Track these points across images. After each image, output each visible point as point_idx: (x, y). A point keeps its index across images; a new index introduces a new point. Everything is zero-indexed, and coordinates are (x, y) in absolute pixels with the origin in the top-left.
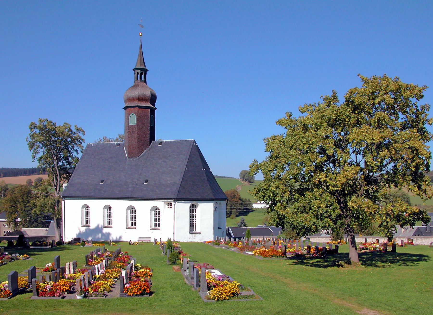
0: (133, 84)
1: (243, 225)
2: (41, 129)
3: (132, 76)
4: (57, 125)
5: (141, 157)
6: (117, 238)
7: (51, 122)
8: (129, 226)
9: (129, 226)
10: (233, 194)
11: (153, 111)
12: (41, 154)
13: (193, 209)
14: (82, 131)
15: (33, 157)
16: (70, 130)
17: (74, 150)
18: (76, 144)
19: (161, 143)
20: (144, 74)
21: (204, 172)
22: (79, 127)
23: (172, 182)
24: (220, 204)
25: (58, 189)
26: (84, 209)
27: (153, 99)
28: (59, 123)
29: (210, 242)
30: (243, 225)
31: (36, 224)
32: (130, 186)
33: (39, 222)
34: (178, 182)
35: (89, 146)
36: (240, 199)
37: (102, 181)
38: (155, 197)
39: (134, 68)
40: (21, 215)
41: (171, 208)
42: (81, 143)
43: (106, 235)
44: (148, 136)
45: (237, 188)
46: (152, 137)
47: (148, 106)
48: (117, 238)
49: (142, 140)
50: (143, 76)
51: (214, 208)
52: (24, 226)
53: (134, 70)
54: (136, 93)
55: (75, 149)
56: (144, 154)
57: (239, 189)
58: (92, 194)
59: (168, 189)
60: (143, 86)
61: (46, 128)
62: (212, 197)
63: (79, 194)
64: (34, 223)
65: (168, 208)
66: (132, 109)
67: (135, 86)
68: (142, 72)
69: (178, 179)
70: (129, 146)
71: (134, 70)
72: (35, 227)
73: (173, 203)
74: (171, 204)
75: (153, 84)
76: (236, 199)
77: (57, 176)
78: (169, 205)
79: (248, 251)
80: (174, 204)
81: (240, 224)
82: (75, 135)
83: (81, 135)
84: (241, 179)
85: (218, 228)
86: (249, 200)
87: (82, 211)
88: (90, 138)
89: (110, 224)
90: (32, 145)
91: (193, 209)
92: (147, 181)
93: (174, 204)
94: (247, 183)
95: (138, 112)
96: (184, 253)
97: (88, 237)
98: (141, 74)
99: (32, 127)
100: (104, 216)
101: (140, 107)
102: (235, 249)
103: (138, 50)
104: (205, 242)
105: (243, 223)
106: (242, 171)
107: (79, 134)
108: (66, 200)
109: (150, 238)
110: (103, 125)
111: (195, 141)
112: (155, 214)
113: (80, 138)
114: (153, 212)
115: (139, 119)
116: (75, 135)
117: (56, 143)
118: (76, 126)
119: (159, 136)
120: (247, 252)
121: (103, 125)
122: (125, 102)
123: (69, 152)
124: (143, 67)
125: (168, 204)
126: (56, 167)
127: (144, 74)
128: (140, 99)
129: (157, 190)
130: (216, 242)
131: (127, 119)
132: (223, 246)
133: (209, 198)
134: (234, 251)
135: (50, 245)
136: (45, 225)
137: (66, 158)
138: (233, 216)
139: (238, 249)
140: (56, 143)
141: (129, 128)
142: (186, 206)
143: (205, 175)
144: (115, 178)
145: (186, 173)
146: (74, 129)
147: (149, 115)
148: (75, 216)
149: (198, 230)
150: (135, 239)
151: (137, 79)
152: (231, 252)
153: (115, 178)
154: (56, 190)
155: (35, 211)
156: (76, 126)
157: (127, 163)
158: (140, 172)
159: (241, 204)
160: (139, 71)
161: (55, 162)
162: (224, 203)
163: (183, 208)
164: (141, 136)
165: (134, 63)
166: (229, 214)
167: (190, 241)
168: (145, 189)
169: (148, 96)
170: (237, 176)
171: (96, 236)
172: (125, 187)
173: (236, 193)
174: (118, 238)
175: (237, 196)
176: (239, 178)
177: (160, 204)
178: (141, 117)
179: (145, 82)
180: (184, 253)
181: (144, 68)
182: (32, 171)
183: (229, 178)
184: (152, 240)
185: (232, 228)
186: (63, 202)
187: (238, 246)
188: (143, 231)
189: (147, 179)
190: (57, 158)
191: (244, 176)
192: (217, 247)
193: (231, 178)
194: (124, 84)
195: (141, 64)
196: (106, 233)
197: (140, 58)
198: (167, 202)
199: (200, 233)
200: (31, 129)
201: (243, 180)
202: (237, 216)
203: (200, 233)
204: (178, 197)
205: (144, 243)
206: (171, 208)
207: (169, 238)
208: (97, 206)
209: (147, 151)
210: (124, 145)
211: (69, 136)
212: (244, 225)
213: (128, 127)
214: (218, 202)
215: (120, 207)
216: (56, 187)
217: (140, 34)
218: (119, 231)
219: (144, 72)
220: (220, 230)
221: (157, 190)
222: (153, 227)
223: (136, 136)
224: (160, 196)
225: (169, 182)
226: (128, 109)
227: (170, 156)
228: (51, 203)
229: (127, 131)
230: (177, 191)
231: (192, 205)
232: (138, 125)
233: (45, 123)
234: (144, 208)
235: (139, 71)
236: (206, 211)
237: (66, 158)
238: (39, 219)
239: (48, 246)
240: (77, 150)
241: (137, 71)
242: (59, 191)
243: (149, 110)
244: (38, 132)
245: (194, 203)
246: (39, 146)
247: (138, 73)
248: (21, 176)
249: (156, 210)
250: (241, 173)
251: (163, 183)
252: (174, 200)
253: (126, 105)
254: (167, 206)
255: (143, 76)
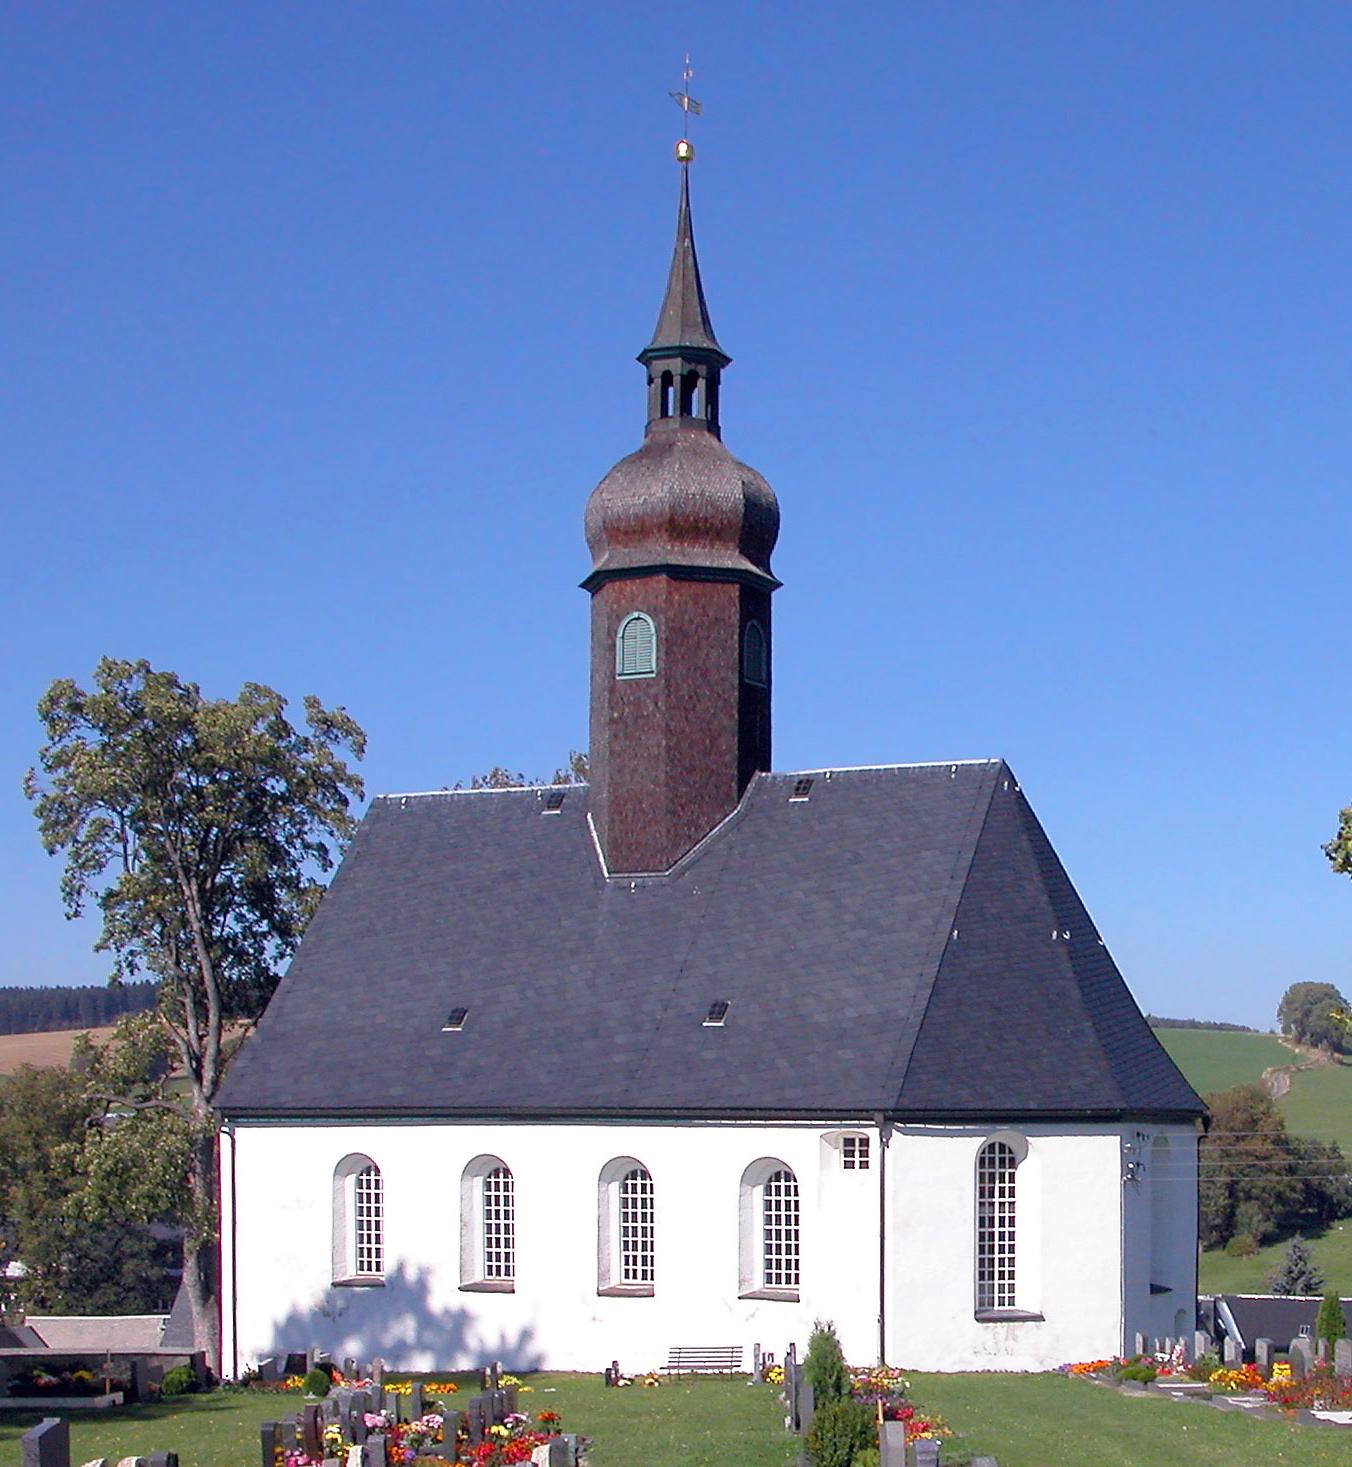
0: (641, 442)
1: (1301, 1283)
2: (111, 724)
3: (636, 393)
4: (208, 697)
5: (687, 868)
6: (503, 1338)
7: (172, 682)
8: (616, 1278)
9: (616, 1278)
10: (1241, 1116)
11: (756, 597)
12: (112, 876)
13: (996, 1167)
14: (349, 729)
15: (72, 892)
16: (281, 729)
17: (307, 846)
18: (314, 809)
19: (804, 785)
20: (701, 383)
21: (1062, 951)
22: (329, 708)
23: (871, 1009)
24: (1161, 1141)
25: (208, 1074)
26: (351, 1179)
27: (758, 527)
28: (219, 687)
29: (1099, 1367)
30: (1301, 1283)
31: (108, 1293)
32: (620, 1040)
33: (130, 1280)
34: (902, 1013)
35: (381, 809)
36: (1281, 1142)
37: (457, 1017)
38: (768, 1100)
39: (646, 343)
40: (31, 1243)
41: (864, 1165)
42: (345, 802)
43: (449, 1325)
44: (729, 745)
45: (1263, 1082)
46: (755, 748)
47: (729, 564)
48: (503, 1338)
49: (691, 769)
50: (698, 396)
51: (1124, 1169)
52: (43, 1306)
53: (645, 358)
54: (657, 491)
55: (309, 838)
56: (706, 853)
57: (1280, 1085)
58: (396, 1091)
59: (846, 1054)
60: (696, 452)
61: (139, 715)
62: (1107, 1096)
63: (317, 1090)
64: (93, 1286)
65: (849, 1165)
66: (631, 587)
67: (653, 453)
68: (691, 376)
69: (905, 993)
70: (617, 805)
71: (645, 358)
72: (105, 1310)
73: (873, 1134)
74: (865, 1142)
75: (763, 439)
76: (1258, 1146)
77: (205, 995)
78: (854, 1153)
79: (1334, 1406)
80: (884, 1144)
81: (1283, 1280)
82: (308, 758)
83: (341, 752)
84: (1286, 1030)
85: (1148, 1289)
86: (1335, 1150)
87: (337, 1193)
88: (396, 770)
89: (498, 1271)
90: (58, 819)
91: (996, 1167)
92: (718, 1010)
93: (884, 1144)
94: (1318, 1055)
95: (669, 601)
96: (118, 881)
97: (339, 1338)
98: (689, 383)
99: (61, 711)
100: (464, 1224)
101: (678, 573)
102: (1248, 1402)
103: (669, 239)
104: (1064, 1370)
105: (1299, 1277)
106: (1295, 989)
107: (332, 747)
108: (240, 1132)
109: (736, 1351)
110: (473, 694)
111: (1005, 771)
112: (768, 1205)
113: (339, 771)
114: (759, 1192)
115: (672, 643)
116: (308, 758)
117: (202, 805)
118: (313, 703)
119: (794, 751)
120: (1321, 1415)
121: (473, 694)
122: (595, 545)
123: (276, 854)
124: (697, 340)
125: (849, 1142)
126: (198, 945)
127: (701, 383)
128: (682, 525)
129: (782, 1063)
130: (1136, 1369)
131: (606, 646)
132: (1177, 1385)
133: (1090, 1105)
134: (1239, 1413)
135: (115, 1388)
136: (157, 1297)
137: (261, 895)
138: (1244, 1238)
139: (1269, 1396)
140: (202, 805)
141: (617, 702)
142: (956, 1154)
143: (1066, 967)
144: (531, 993)
145: (950, 956)
146: (300, 723)
147: (735, 619)
148: (286, 1214)
149: (1024, 1302)
150: (643, 1358)
151: (664, 413)
152: (1226, 1415)
153: (531, 993)
154: (198, 1076)
155: (79, 1204)
156: (313, 703)
157: (604, 908)
158: (679, 958)
159: (1291, 1170)
160: (676, 366)
161: (194, 911)
162: (1181, 1139)
163: (937, 1165)
164: (684, 745)
165: (648, 317)
166: (1220, 1232)
167: (978, 1364)
168: (709, 1055)
169: (726, 507)
170: (1264, 1017)
171: (385, 1329)
172: (590, 1045)
173: (1262, 1107)
174: (513, 1338)
175: (1266, 1128)
176: (1279, 1031)
177: (802, 1147)
178: (685, 635)
179: (713, 426)
180: (118, 881)
181: (712, 346)
182: (110, 1003)
183: (1221, 1027)
184: (748, 1365)
185: (1233, 1303)
186: (225, 1140)
187: (1271, 1386)
188: (704, 1310)
189: (720, 996)
190: (201, 889)
191: (1307, 1014)
192: (1135, 1393)
193: (1234, 1028)
194: (590, 454)
195: (685, 325)
196: (447, 1312)
197: (678, 288)
198: (841, 1132)
199: (1039, 1318)
200: (53, 723)
201: (1298, 1041)
202: (1266, 1240)
203: (1039, 1318)
204: (906, 1103)
205: (699, 1385)
206: (864, 1165)
207: (824, 1320)
208: (425, 1167)
209: (720, 835)
210: (584, 801)
211: (275, 762)
212: (1308, 1289)
213: (612, 690)
214: (1152, 1130)
215: (559, 1166)
216: (198, 1059)
217: (683, 150)
218: (564, 1319)
219: (702, 370)
220: (1161, 1298)
221: (782, 1063)
222: (758, 1283)
223: (657, 741)
224: (794, 1096)
225: (850, 1013)
226: (610, 590)
227: (857, 859)
228: (171, 1156)
229: (604, 719)
230: (902, 1064)
231: (992, 1147)
232: (666, 674)
233: (136, 685)
234: (701, 1169)
235: (676, 366)
236: (1075, 1184)
237: (261, 895)
238: (128, 1266)
239: (102, 1392)
240: (322, 849)
241: (660, 366)
242: (215, 1083)
243: (734, 591)
244: (94, 739)
245: (1004, 1134)
246: (103, 827)
247: (667, 378)
248: (45, 1029)
249: (777, 1179)
250: (1289, 1001)
251: (821, 1018)
252: (879, 1116)
253: (599, 565)
254: (838, 1157)
255: (698, 396)
